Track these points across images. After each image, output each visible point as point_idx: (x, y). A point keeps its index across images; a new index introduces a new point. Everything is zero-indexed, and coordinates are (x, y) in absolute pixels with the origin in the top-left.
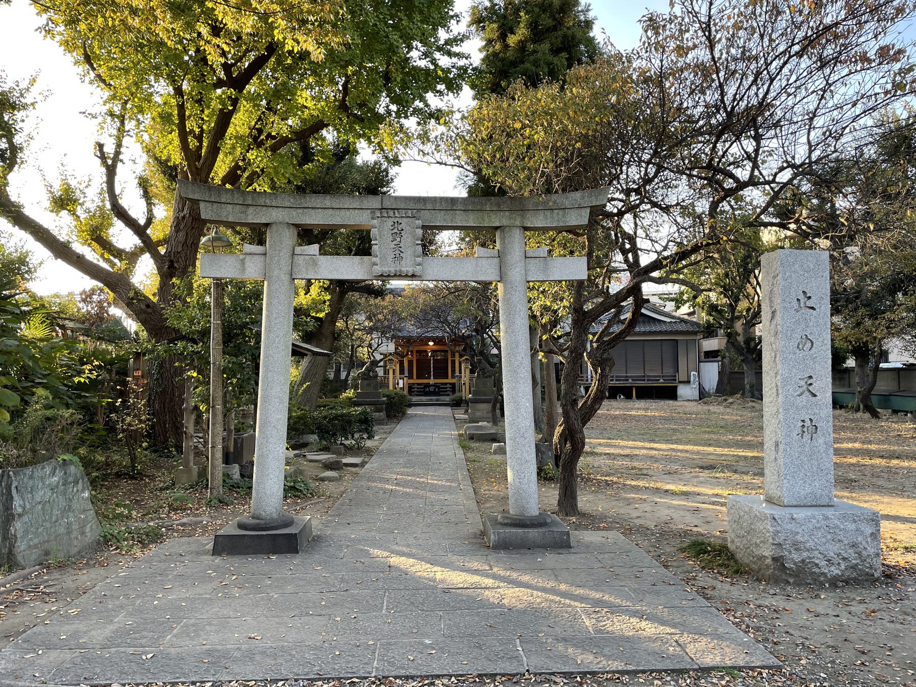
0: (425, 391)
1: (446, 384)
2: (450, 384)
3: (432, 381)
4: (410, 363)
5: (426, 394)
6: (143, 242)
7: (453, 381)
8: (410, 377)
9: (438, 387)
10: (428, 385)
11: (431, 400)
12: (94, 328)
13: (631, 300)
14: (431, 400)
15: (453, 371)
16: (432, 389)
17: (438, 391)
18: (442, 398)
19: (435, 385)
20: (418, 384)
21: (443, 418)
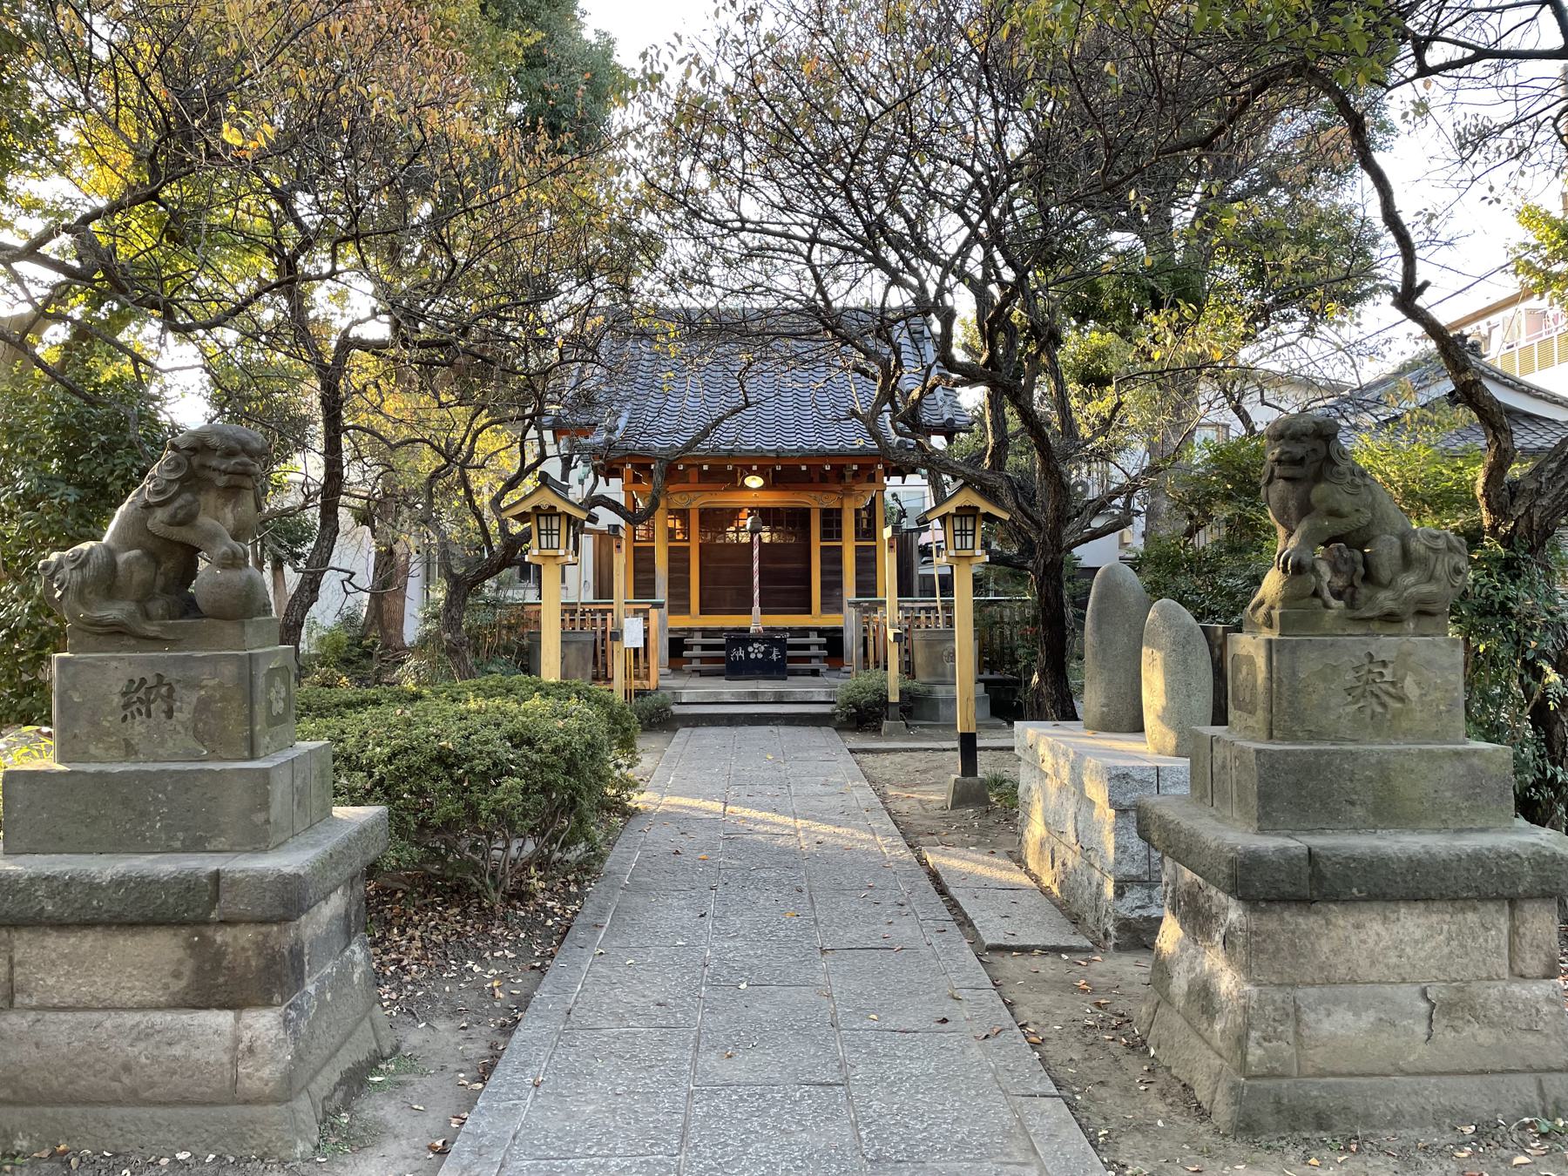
0: (733, 658)
1: (804, 632)
2: (821, 632)
3: (756, 621)
4: (678, 559)
5: (736, 670)
6: (66, 274)
7: (830, 621)
8: (678, 603)
9: (781, 644)
10: (741, 638)
11: (755, 699)
12: (1240, 328)
13: (43, 250)
14: (755, 699)
15: (832, 585)
16: (756, 651)
17: (777, 657)
18: (794, 686)
19: (771, 638)
20: (706, 632)
21: (799, 876)
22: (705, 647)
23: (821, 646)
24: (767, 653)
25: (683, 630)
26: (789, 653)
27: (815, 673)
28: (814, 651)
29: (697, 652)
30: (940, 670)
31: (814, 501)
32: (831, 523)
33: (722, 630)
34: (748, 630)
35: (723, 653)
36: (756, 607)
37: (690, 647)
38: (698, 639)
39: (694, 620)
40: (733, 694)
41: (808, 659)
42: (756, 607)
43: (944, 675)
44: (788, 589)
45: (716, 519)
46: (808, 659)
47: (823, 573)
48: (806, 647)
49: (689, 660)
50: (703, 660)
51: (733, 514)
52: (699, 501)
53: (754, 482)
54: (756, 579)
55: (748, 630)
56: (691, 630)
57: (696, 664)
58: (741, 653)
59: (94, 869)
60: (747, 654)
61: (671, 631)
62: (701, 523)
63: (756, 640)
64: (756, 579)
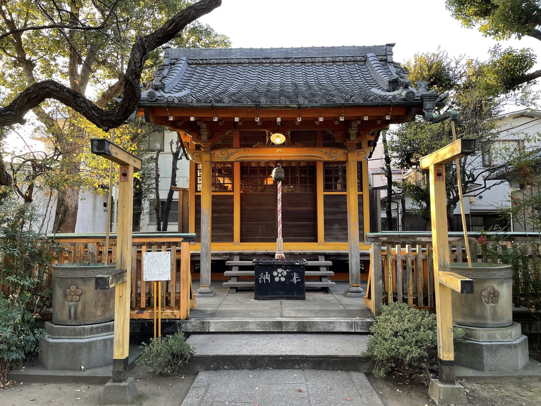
1: (315, 256)
2: (327, 256)
3: (280, 248)
5: (264, 291)
8: (221, 231)
10: (266, 264)
16: (280, 275)
19: (292, 263)
20: (243, 256)
22: (241, 268)
23: (329, 268)
24: (289, 277)
25: (226, 254)
26: (307, 273)
27: (325, 290)
28: (323, 272)
29: (235, 272)
30: (478, 311)
31: (321, 155)
32: (335, 175)
33: (254, 255)
34: (273, 255)
35: (252, 272)
36: (280, 238)
37: (230, 268)
38: (236, 261)
39: (236, 246)
40: (258, 324)
41: (320, 278)
42: (280, 238)
43: (483, 317)
44: (301, 226)
45: (252, 172)
46: (320, 278)
47: (325, 213)
48: (317, 268)
49: (230, 278)
50: (239, 278)
51: (266, 170)
52: (237, 155)
53: (278, 139)
54: (280, 217)
55: (273, 255)
56: (231, 255)
57: (233, 282)
58: (267, 277)
59: (353, 217)
60: (273, 277)
61: (213, 255)
62: (242, 179)
63: (279, 266)
64: (280, 217)
